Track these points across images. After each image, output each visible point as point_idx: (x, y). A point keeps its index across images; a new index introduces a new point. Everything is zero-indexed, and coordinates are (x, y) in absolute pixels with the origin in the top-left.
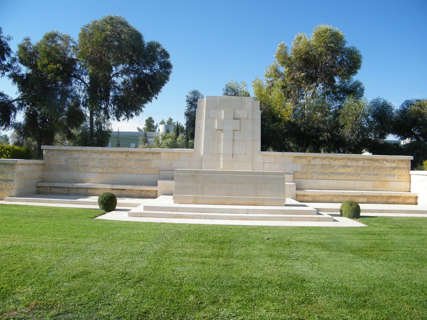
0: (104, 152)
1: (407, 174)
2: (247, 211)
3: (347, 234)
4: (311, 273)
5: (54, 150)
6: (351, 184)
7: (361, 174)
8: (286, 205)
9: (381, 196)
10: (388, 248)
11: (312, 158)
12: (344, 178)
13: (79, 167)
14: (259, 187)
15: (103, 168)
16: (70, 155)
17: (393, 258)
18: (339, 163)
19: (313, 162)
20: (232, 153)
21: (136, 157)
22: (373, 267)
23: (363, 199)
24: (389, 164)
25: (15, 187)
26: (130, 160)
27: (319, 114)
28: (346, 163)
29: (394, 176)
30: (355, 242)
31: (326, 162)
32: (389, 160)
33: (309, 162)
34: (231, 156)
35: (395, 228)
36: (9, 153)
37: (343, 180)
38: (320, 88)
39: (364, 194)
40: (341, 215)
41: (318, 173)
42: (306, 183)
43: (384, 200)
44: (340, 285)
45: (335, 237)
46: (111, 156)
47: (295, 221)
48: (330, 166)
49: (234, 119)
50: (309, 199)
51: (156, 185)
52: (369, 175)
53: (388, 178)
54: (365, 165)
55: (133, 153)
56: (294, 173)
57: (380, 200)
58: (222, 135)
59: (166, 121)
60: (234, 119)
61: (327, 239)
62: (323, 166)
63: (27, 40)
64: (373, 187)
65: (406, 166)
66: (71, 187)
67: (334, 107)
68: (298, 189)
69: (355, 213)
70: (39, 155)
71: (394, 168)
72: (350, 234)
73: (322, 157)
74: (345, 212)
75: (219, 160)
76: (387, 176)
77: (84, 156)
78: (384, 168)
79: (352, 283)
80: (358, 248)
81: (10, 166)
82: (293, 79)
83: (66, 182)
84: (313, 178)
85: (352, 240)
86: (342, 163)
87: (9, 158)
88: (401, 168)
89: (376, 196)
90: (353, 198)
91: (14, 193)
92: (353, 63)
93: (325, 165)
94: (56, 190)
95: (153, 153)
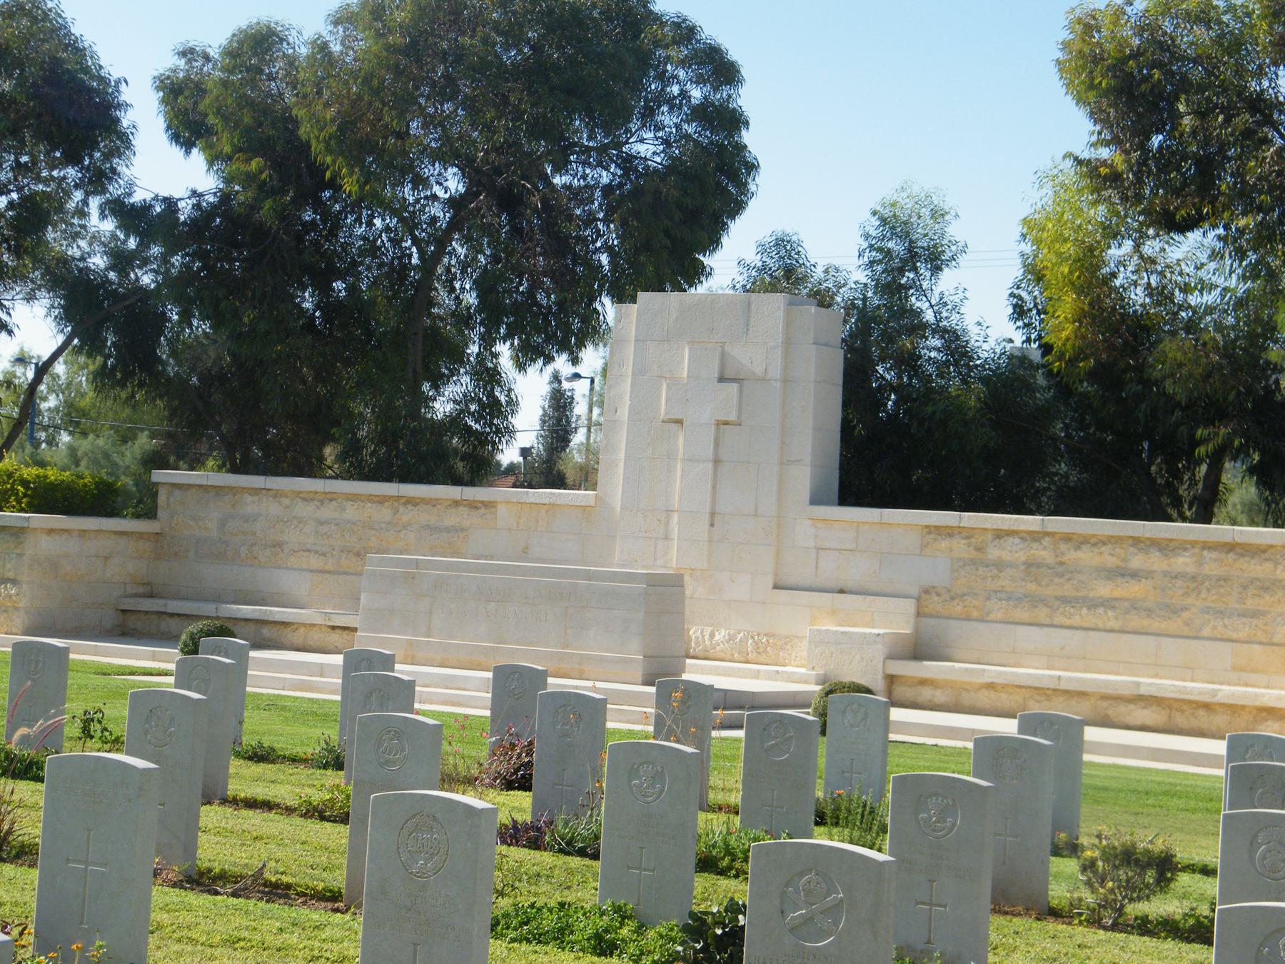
7: (1185, 609)
11: (990, 536)
15: (324, 555)
16: (234, 506)
23: (1145, 712)
26: (406, 526)
31: (1042, 553)
33: (979, 549)
34: (707, 523)
36: (25, 495)
37: (1112, 631)
39: (1143, 691)
41: (1009, 599)
46: (351, 512)
48: (1062, 570)
50: (940, 696)
52: (1221, 614)
54: (1206, 570)
55: (415, 505)
60: (722, 379)
62: (1031, 566)
70: (145, 503)
77: (274, 508)
81: (12, 535)
84: (992, 617)
86: (1108, 558)
87: (22, 510)
89: (1207, 706)
90: (1105, 704)
93: (1039, 566)
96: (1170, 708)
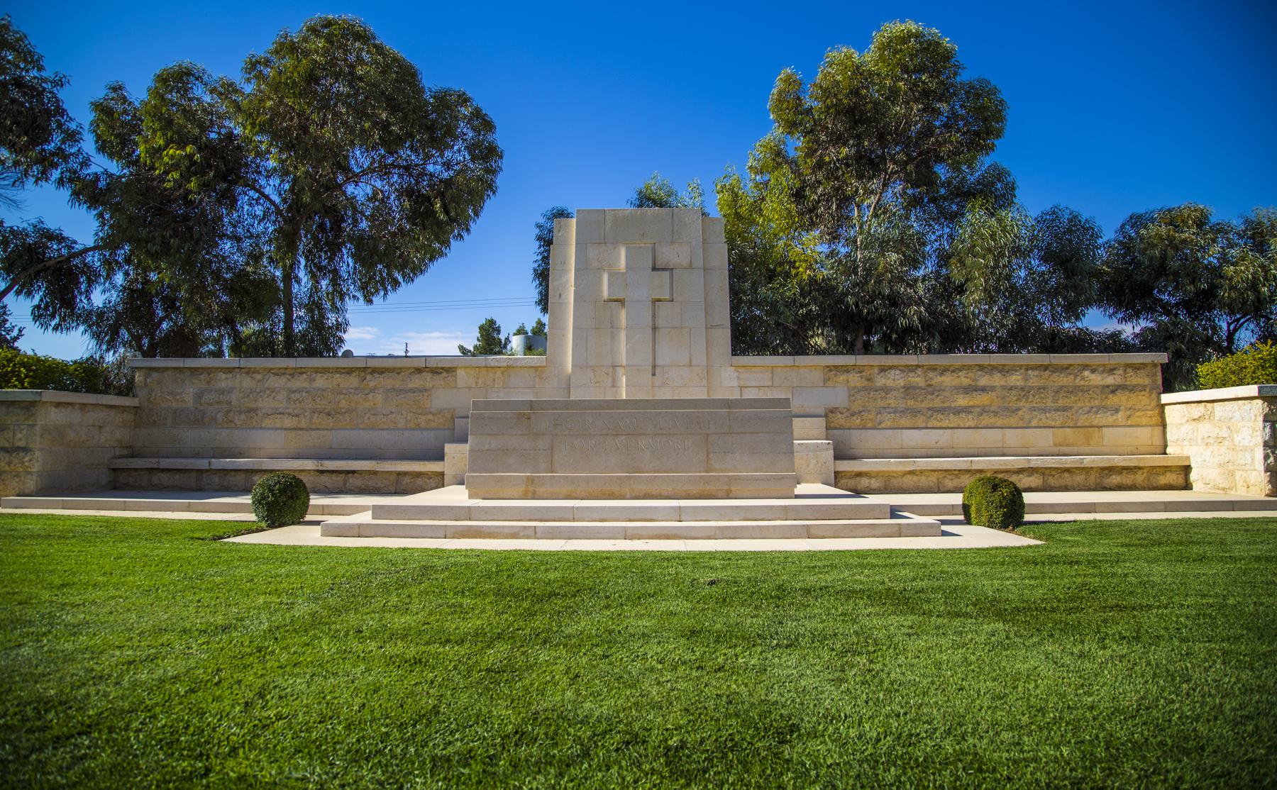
0: (301, 371)
1: (1154, 403)
2: (679, 514)
3: (983, 564)
4: (832, 697)
5: (166, 369)
6: (990, 437)
8: (797, 497)
9: (1083, 468)
10: (1132, 601)
11: (876, 371)
14: (713, 442)
16: (208, 383)
17: (1162, 632)
18: (956, 382)
19: (880, 381)
22: (1087, 665)
24: (1099, 378)
25: (36, 468)
26: (373, 390)
27: (894, 256)
29: (1117, 411)
30: (1013, 585)
31: (917, 379)
32: (1100, 365)
33: (869, 380)
35: (1142, 546)
36: (26, 376)
38: (894, 194)
39: (1033, 465)
40: (968, 521)
41: (895, 412)
42: (863, 439)
43: (1092, 479)
44: (949, 747)
45: (942, 572)
47: (824, 537)
48: (931, 390)
49: (654, 269)
51: (440, 457)
52: (1044, 410)
53: (1099, 419)
54: (1030, 383)
56: (829, 413)
57: (1079, 478)
58: (623, 314)
59: (529, 329)
60: (654, 269)
61: (914, 579)
63: (117, 88)
64: (1055, 445)
65: (1147, 381)
67: (933, 237)
68: (838, 457)
69: (1011, 514)
71: (1114, 390)
72: (994, 564)
73: (906, 366)
74: (978, 510)
76: (1096, 413)
77: (247, 383)
78: (1085, 390)
79: (1006, 736)
80: (1023, 601)
82: (820, 165)
83: (197, 455)
84: (883, 425)
85: (1002, 579)
86: (963, 379)
88: (1135, 386)
89: (1067, 470)
91: (31, 484)
92: (984, 120)
94: (165, 479)
96: (1043, 474)
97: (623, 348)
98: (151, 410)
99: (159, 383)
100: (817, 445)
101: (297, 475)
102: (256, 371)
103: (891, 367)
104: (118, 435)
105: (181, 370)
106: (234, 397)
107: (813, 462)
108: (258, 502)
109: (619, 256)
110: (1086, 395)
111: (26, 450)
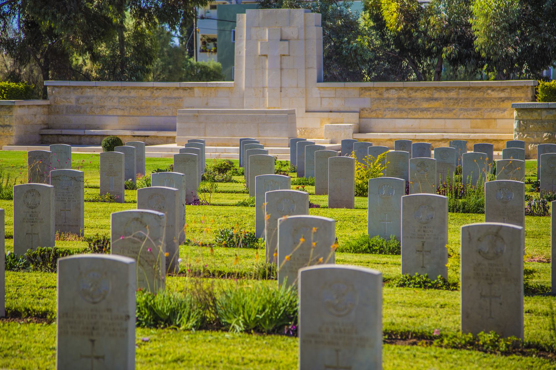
0: (124, 88)
5: (62, 86)
11: (384, 90)
12: (429, 116)
13: (93, 109)
15: (123, 110)
18: (423, 95)
19: (386, 95)
20: (279, 86)
21: (163, 93)
26: (157, 98)
28: (432, 95)
29: (505, 110)
31: (403, 94)
32: (497, 87)
33: (380, 94)
36: (4, 93)
39: (445, 137)
41: (392, 110)
46: (133, 93)
52: (466, 110)
53: (495, 115)
54: (460, 96)
55: (161, 90)
58: (267, 63)
64: (471, 128)
66: (83, 134)
73: (399, 88)
75: (263, 96)
76: (493, 112)
77: (100, 93)
78: (488, 100)
81: (7, 108)
83: (78, 128)
84: (386, 117)
86: (427, 94)
87: (5, 99)
91: (13, 140)
93: (402, 98)
95: (184, 89)
97: (267, 78)
98: (56, 106)
99: (59, 93)
100: (345, 126)
101: (120, 138)
102: (103, 88)
103: (392, 88)
104: (42, 118)
105: (69, 87)
106: (94, 100)
107: (343, 134)
108: (104, 147)
109: (265, 34)
110: (489, 103)
111: (9, 126)
